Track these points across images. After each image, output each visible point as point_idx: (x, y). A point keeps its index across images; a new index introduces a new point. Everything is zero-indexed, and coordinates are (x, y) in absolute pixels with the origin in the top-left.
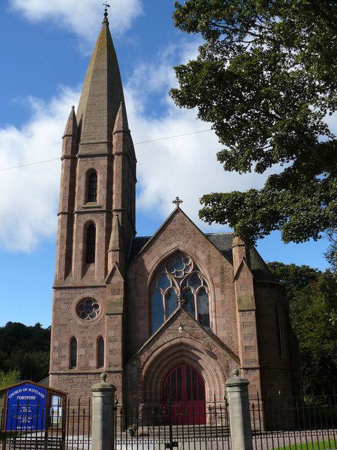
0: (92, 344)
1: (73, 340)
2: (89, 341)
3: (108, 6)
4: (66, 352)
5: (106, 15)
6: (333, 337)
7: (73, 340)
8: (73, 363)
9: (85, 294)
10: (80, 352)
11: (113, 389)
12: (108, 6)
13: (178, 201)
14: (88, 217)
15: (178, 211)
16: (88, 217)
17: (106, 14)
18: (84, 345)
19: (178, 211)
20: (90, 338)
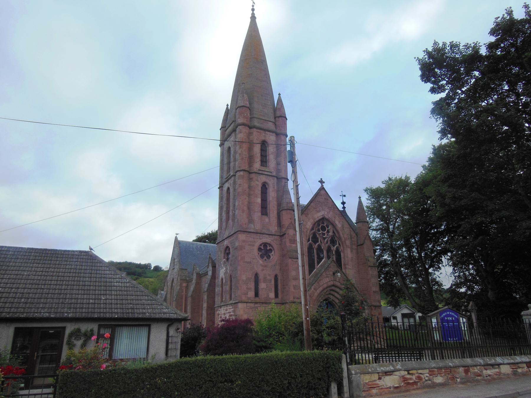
0: (271, 281)
1: (256, 276)
2: (269, 278)
3: (345, 196)
4: (252, 285)
5: (253, 10)
6: (530, 150)
7: (256, 276)
8: (257, 294)
9: (263, 240)
10: (262, 285)
11: (71, 368)
12: (345, 196)
13: (321, 182)
14: (263, 179)
15: (322, 189)
16: (263, 179)
17: (253, 10)
18: (265, 280)
19: (322, 189)
20: (269, 275)
